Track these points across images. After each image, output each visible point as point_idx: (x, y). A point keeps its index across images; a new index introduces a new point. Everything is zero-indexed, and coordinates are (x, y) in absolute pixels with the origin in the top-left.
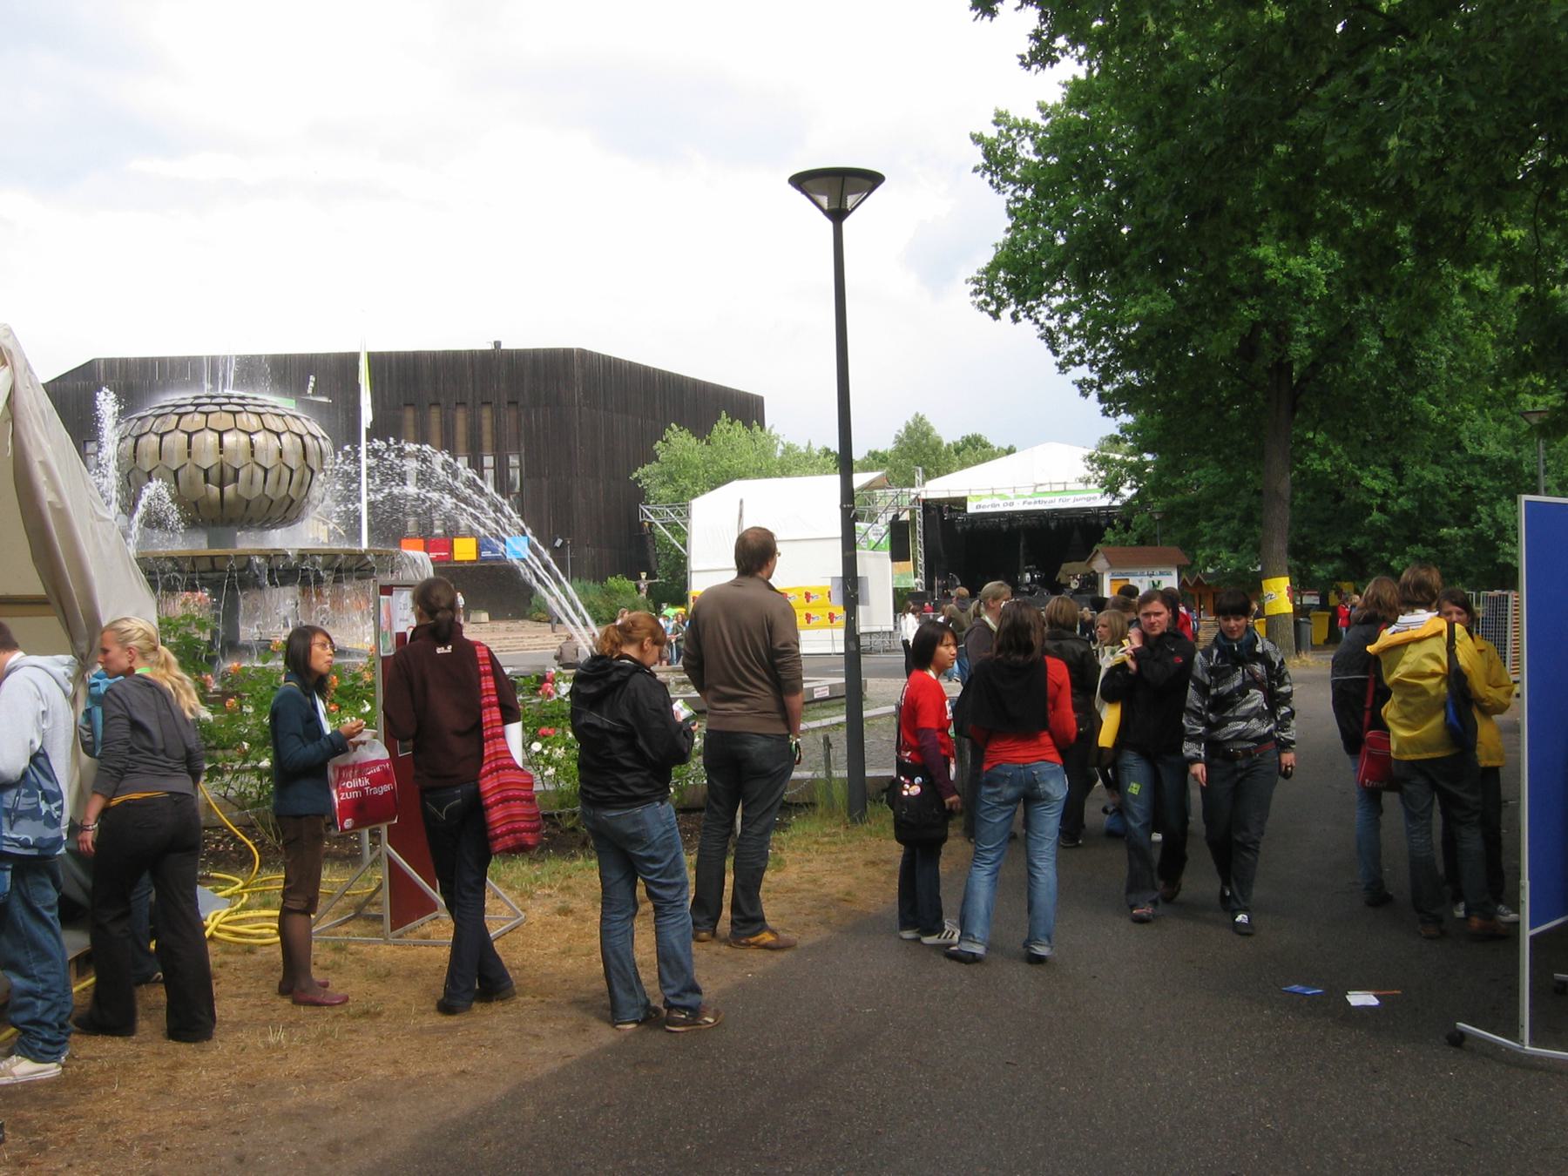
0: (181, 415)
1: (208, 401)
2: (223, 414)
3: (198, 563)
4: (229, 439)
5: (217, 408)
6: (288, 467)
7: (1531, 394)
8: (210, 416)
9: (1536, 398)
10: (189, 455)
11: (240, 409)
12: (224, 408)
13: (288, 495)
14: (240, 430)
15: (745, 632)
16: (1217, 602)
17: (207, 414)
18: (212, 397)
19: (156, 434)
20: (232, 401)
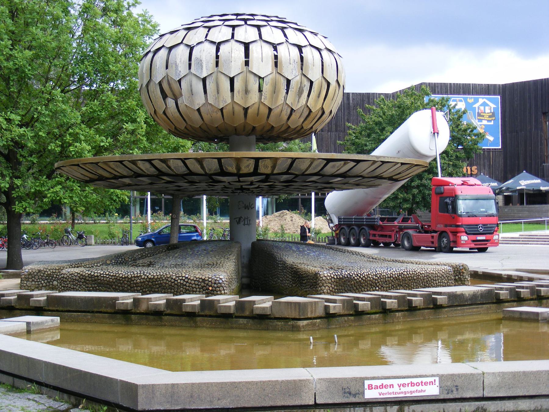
0: (209, 28)
1: (234, 17)
2: (248, 27)
3: (261, 163)
4: (282, 51)
5: (243, 23)
6: (255, 75)
7: (79, 36)
8: (236, 29)
9: (132, 37)
10: (247, 63)
11: (265, 23)
12: (249, 22)
13: (260, 102)
14: (237, 41)
15: (491, 176)
16: (373, 146)
17: (234, 27)
18: (237, 15)
19: (187, 45)
20: (256, 17)
